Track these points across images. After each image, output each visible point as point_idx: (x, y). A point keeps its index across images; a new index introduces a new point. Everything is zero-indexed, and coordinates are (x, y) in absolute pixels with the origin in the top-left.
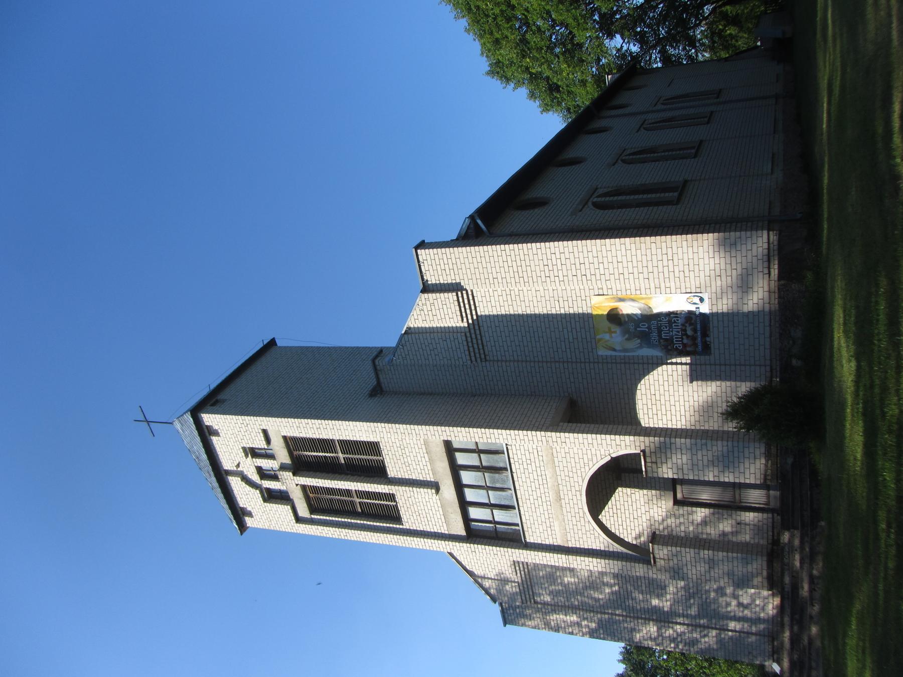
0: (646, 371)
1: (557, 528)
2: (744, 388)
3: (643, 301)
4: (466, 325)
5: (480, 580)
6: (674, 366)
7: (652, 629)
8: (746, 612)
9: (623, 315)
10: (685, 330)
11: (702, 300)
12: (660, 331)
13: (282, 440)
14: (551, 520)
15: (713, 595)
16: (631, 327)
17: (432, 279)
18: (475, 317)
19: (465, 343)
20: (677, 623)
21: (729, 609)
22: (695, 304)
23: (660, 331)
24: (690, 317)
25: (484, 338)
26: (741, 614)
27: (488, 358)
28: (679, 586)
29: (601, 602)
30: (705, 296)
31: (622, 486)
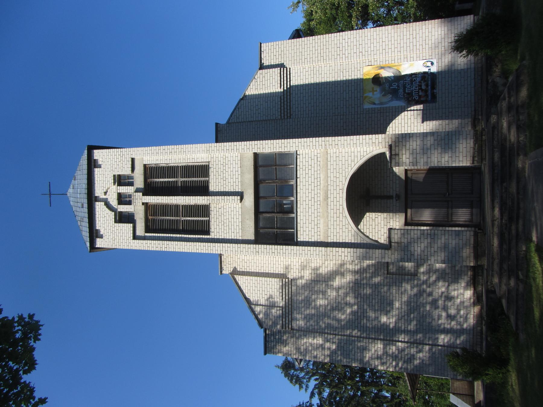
0: (394, 117)
1: (321, 226)
2: (466, 22)
3: (395, 68)
4: (282, 90)
5: (253, 306)
6: (412, 112)
7: (379, 346)
8: (453, 323)
9: (382, 77)
10: (421, 86)
11: (432, 64)
12: (405, 87)
13: (142, 168)
14: (319, 218)
15: (428, 308)
16: (387, 86)
17: (266, 62)
18: (288, 86)
19: (279, 103)
20: (399, 341)
21: (440, 322)
22: (428, 67)
23: (405, 87)
24: (425, 76)
25: (292, 109)
26: (449, 326)
27: (292, 116)
28: (403, 300)
29: (343, 323)
30: (435, 61)
31: (369, 211)
